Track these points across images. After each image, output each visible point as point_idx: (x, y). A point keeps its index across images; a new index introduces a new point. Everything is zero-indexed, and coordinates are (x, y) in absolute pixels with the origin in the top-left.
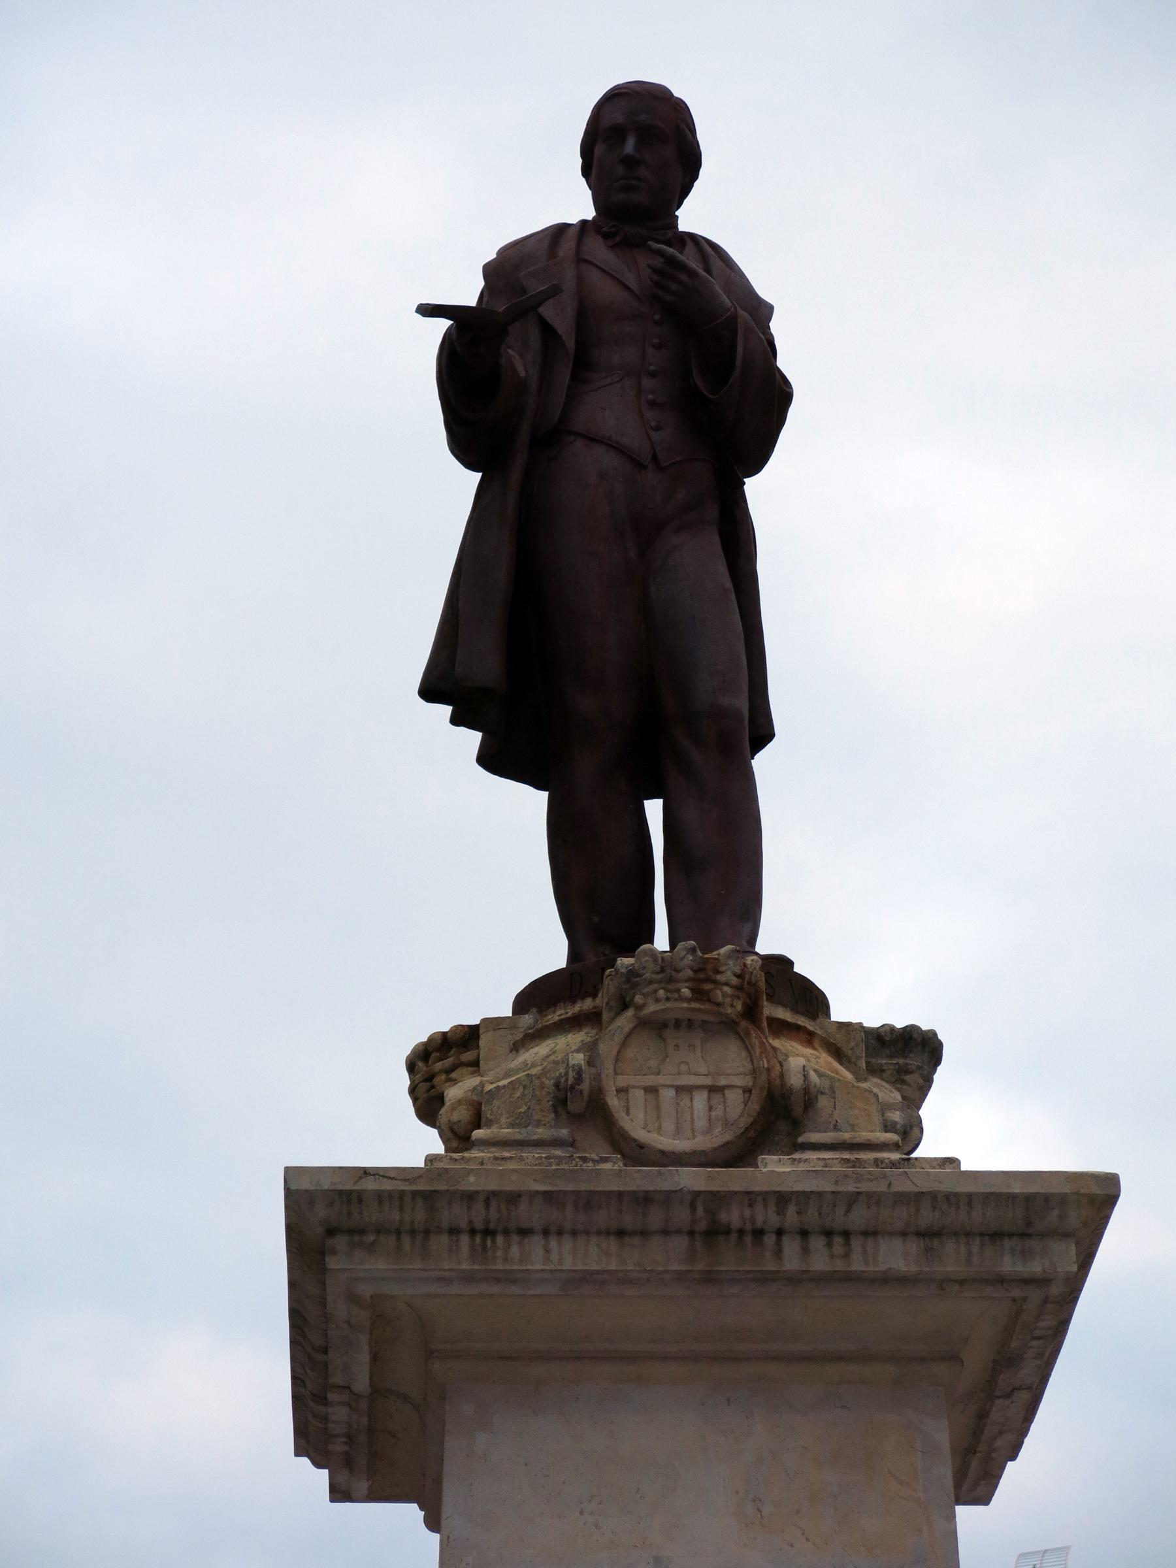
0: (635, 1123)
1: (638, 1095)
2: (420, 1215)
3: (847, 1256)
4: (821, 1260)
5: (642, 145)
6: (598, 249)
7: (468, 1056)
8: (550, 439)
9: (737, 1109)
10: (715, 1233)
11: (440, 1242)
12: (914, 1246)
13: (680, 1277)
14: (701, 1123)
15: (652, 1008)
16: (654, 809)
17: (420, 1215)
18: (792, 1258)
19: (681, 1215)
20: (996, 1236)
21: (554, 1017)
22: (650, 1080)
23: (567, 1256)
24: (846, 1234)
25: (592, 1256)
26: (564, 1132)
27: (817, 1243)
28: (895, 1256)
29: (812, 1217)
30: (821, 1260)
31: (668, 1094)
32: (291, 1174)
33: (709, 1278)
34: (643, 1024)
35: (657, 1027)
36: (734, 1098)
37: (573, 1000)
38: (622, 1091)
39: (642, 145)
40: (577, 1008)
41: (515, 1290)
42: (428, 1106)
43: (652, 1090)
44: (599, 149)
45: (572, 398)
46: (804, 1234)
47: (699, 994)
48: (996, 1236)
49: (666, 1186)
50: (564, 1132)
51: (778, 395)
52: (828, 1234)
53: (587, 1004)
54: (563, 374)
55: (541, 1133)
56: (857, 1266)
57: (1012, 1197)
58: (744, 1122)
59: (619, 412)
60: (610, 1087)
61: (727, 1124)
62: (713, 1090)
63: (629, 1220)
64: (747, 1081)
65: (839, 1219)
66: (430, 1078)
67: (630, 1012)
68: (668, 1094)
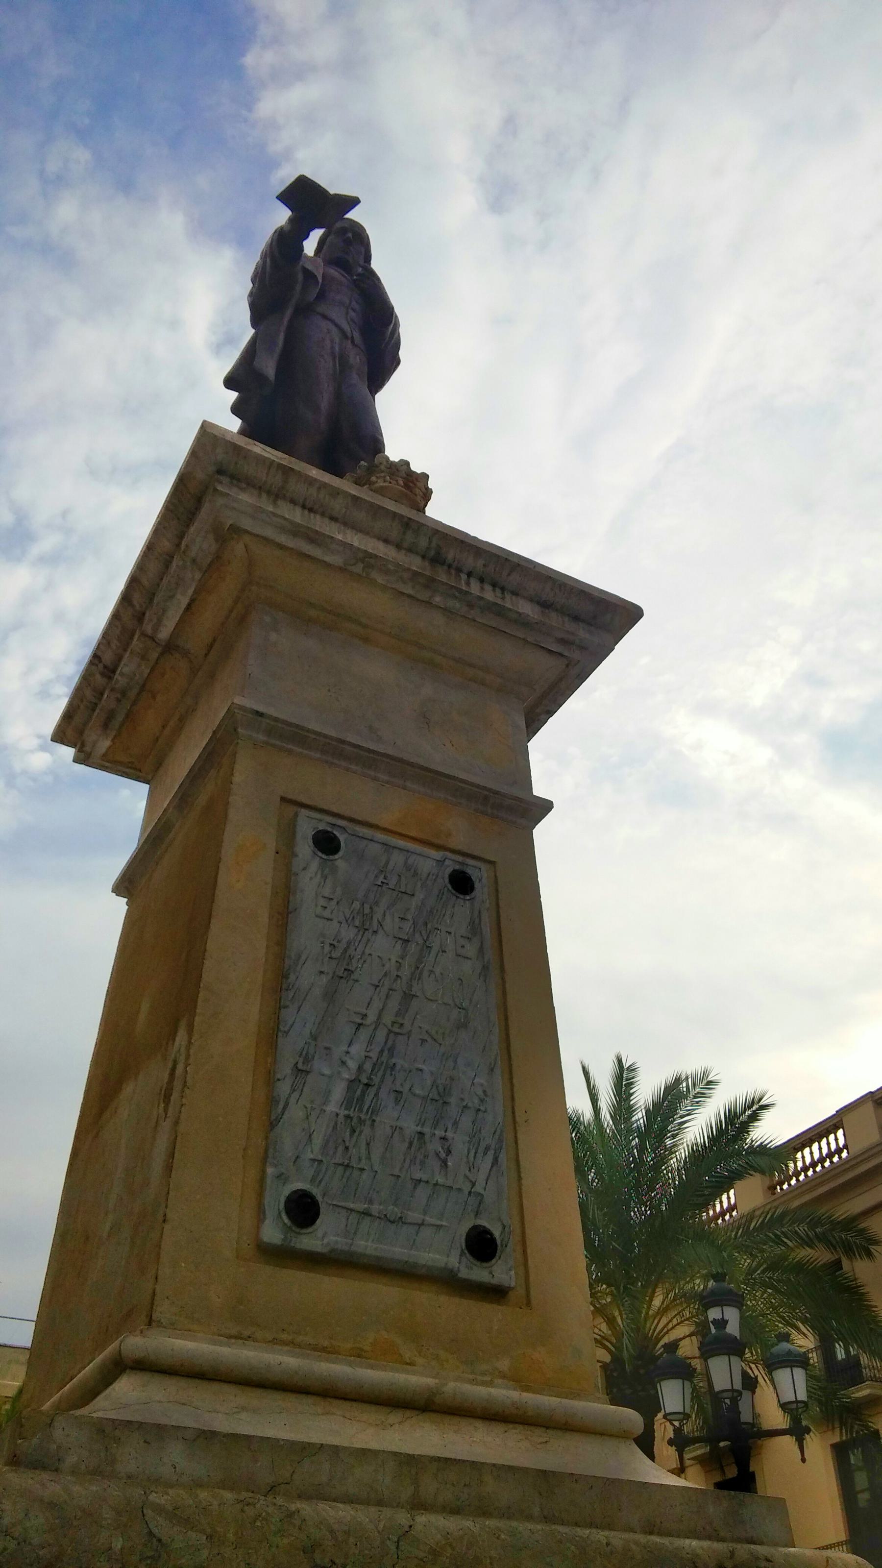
3: (503, 598)
12: (537, 608)
19: (423, 543)
27: (488, 587)
28: (526, 608)
30: (489, 595)
32: (204, 422)
59: (337, 319)
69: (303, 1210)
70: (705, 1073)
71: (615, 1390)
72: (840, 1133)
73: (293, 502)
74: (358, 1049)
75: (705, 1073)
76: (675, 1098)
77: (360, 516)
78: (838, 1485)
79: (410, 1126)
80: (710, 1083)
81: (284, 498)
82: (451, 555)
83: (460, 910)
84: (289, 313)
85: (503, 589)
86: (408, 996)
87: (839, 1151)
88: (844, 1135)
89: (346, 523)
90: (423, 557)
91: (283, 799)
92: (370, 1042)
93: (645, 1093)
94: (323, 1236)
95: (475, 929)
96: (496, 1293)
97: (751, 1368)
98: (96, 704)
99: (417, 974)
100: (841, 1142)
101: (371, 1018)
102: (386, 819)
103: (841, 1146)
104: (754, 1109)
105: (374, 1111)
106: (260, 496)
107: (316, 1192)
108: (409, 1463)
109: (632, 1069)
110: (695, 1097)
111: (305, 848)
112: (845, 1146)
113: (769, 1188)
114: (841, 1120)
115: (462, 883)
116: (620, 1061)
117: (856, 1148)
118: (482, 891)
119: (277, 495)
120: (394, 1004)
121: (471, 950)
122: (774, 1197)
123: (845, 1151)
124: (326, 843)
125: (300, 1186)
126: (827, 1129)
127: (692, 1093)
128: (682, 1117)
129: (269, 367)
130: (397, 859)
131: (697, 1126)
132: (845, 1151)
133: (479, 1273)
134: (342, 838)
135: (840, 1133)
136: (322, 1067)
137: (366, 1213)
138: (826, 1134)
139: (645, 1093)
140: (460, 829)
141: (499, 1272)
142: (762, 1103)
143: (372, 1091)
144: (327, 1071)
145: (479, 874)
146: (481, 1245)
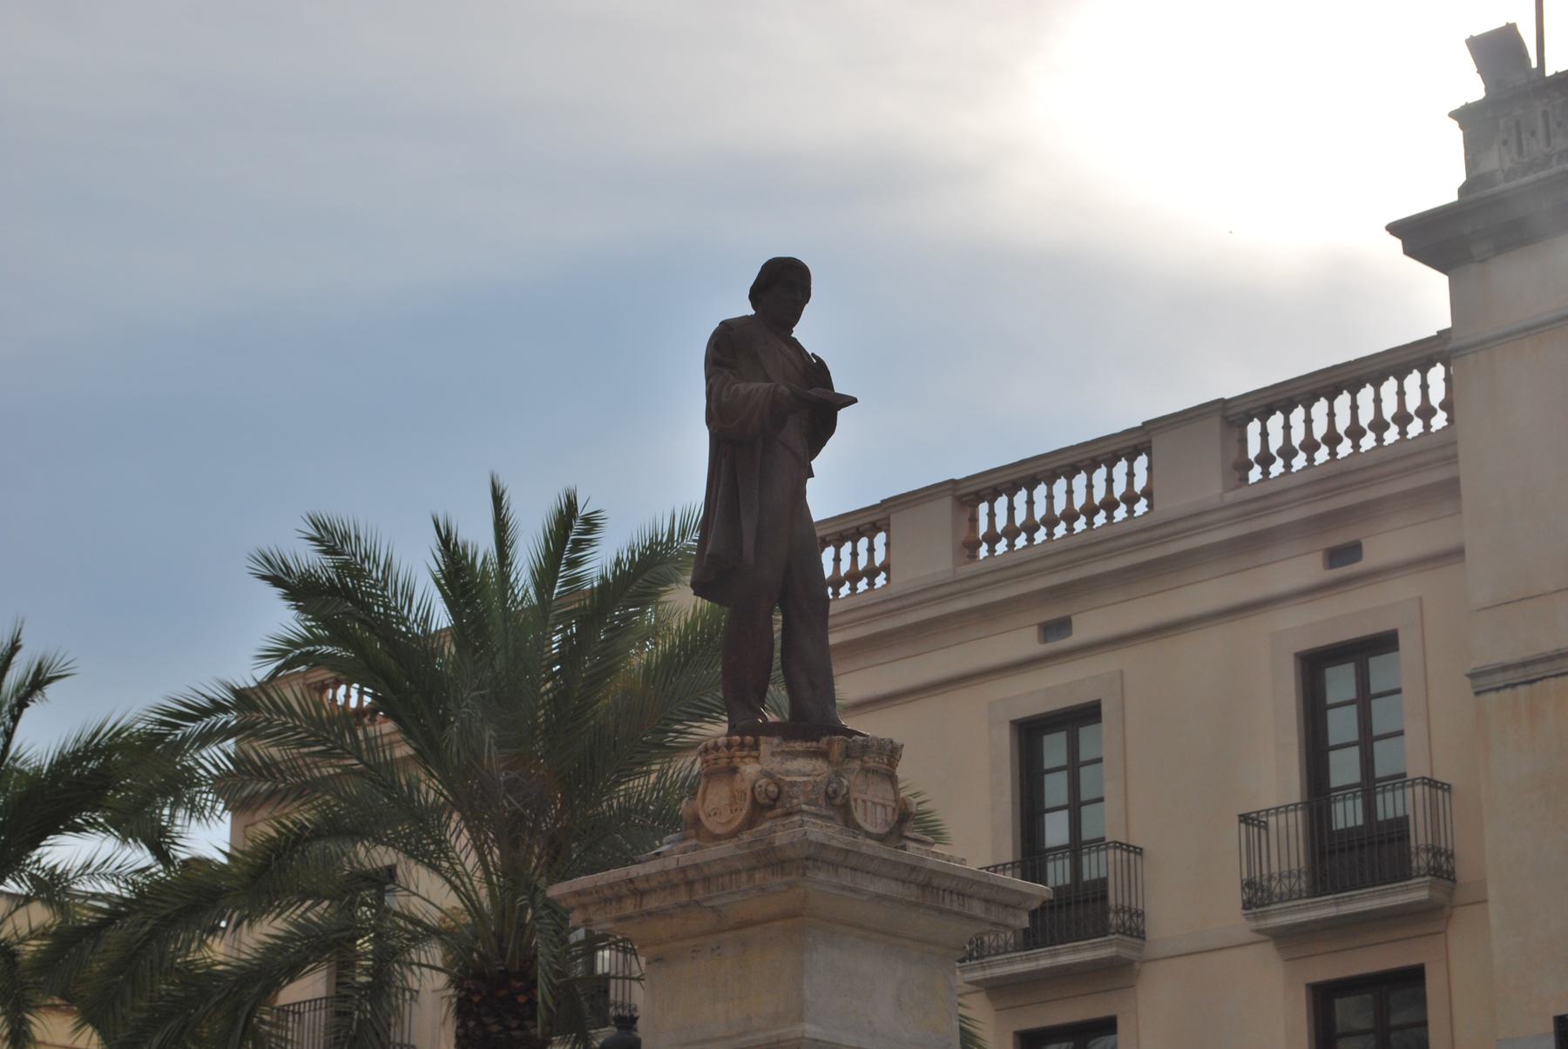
0: (858, 815)
7: (755, 753)
35: (866, 771)
36: (890, 810)
66: (731, 758)
71: (471, 1024)
72: (880, 539)
78: (1013, 803)
81: (891, 833)
82: (936, 882)
87: (871, 573)
88: (1149, 469)
97: (490, 758)
100: (1140, 483)
103: (1077, 506)
112: (885, 567)
114: (888, 518)
117: (1170, 506)
122: (968, 569)
123: (883, 575)
126: (857, 528)
132: (883, 575)
138: (871, 530)
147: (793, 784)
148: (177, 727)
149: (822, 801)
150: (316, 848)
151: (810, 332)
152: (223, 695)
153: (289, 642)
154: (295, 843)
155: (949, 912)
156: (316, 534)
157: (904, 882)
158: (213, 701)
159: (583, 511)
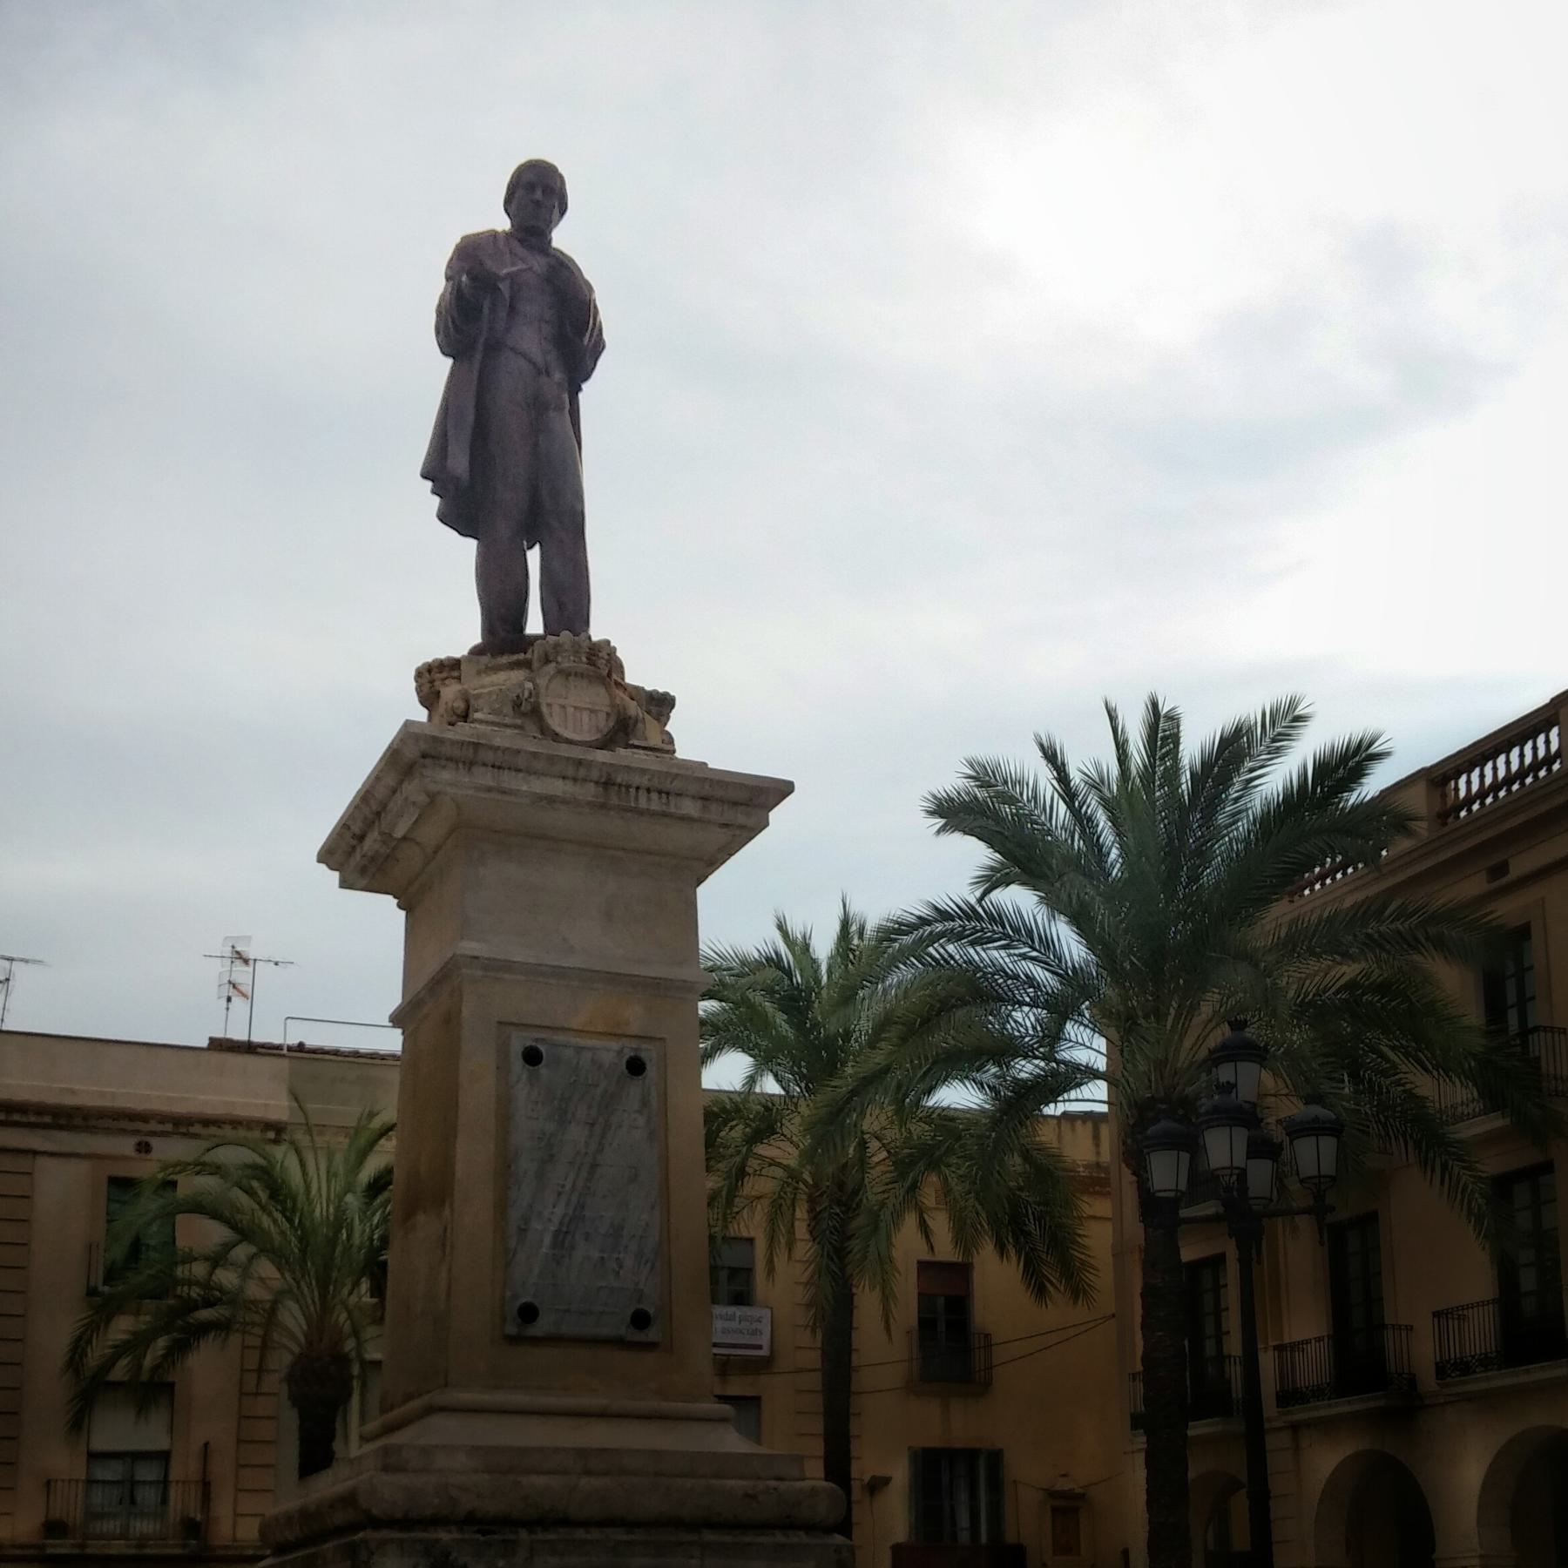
0: (555, 723)
1: (556, 708)
2: (470, 753)
3: (668, 804)
4: (656, 804)
5: (537, 193)
6: (515, 244)
7: (456, 674)
8: (494, 347)
9: (605, 724)
10: (608, 784)
11: (477, 770)
12: (699, 803)
13: (589, 804)
14: (586, 727)
15: (566, 665)
16: (534, 557)
17: (470, 753)
18: (643, 803)
19: (595, 775)
20: (735, 804)
21: (504, 660)
22: (562, 701)
23: (538, 786)
24: (668, 794)
25: (557, 787)
26: (519, 722)
27: (654, 796)
28: (689, 807)
29: (656, 783)
30: (656, 804)
31: (570, 710)
33: (603, 806)
34: (560, 672)
35: (566, 674)
36: (602, 716)
37: (513, 653)
38: (549, 705)
39: (537, 193)
40: (515, 657)
41: (507, 798)
42: (428, 697)
43: (563, 707)
44: (520, 193)
45: (507, 330)
46: (649, 791)
47: (591, 662)
48: (735, 804)
49: (590, 758)
50: (519, 722)
51: (598, 347)
52: (660, 792)
53: (521, 656)
54: (503, 314)
55: (507, 721)
56: (673, 810)
57: (746, 786)
58: (606, 730)
59: (531, 338)
60: (543, 701)
61: (598, 730)
62: (592, 711)
63: (570, 771)
64: (608, 709)
65: (667, 786)
66: (432, 682)
67: (553, 665)
68: (570, 710)
69: (529, 1313)
70: (1293, 704)
73: (484, 765)
74: (559, 1211)
75: (1293, 704)
76: (1235, 751)
77: (539, 765)
79: (596, 1255)
80: (1298, 719)
83: (635, 1089)
84: (478, 356)
85: (668, 794)
86: (594, 1166)
89: (530, 772)
90: (597, 783)
91: (500, 1023)
92: (567, 1204)
93: (1194, 745)
94: (542, 1326)
95: (645, 1103)
96: (651, 1346)
98: (354, 847)
99: (600, 1150)
101: (567, 1188)
102: (576, 1022)
104: (1351, 761)
105: (572, 1247)
106: (457, 769)
107: (536, 1302)
108: (583, 1453)
109: (1173, 718)
110: (1274, 741)
111: (518, 1064)
112: (1558, 754)
113: (1439, 816)
115: (636, 1067)
116: (1155, 705)
118: (651, 1070)
119: (470, 765)
120: (584, 1174)
121: (641, 1121)
124: (532, 1057)
125: (524, 1300)
127: (1270, 733)
128: (1252, 770)
129: (459, 463)
130: (587, 1056)
131: (1276, 778)
133: (639, 1337)
134: (542, 1048)
135: (1554, 732)
136: (536, 1225)
137: (568, 1311)
139: (1194, 745)
140: (635, 1016)
141: (652, 1334)
142: (1373, 750)
143: (569, 1237)
144: (539, 1227)
145: (649, 1053)
146: (641, 1320)
147: (478, 697)
148: (895, 940)
149: (508, 709)
150: (960, 1014)
151: (563, 238)
152: (925, 911)
153: (992, 868)
154: (940, 1010)
155: (653, 814)
156: (972, 773)
157: (575, 780)
158: (919, 918)
159: (1164, 709)
